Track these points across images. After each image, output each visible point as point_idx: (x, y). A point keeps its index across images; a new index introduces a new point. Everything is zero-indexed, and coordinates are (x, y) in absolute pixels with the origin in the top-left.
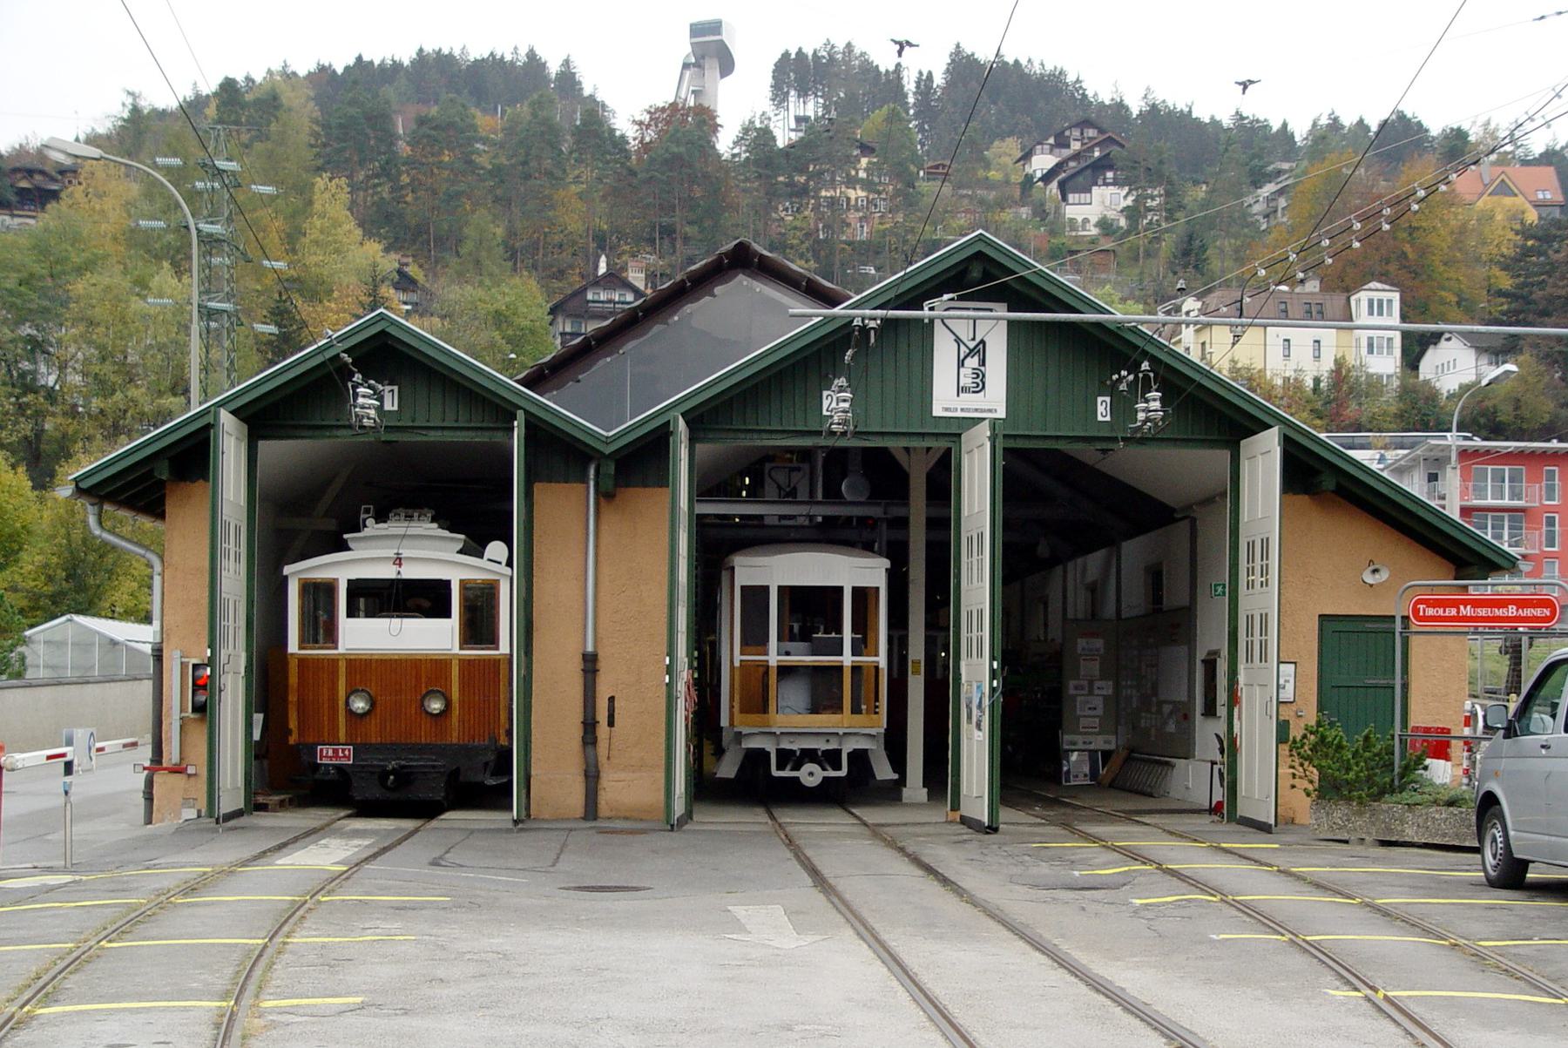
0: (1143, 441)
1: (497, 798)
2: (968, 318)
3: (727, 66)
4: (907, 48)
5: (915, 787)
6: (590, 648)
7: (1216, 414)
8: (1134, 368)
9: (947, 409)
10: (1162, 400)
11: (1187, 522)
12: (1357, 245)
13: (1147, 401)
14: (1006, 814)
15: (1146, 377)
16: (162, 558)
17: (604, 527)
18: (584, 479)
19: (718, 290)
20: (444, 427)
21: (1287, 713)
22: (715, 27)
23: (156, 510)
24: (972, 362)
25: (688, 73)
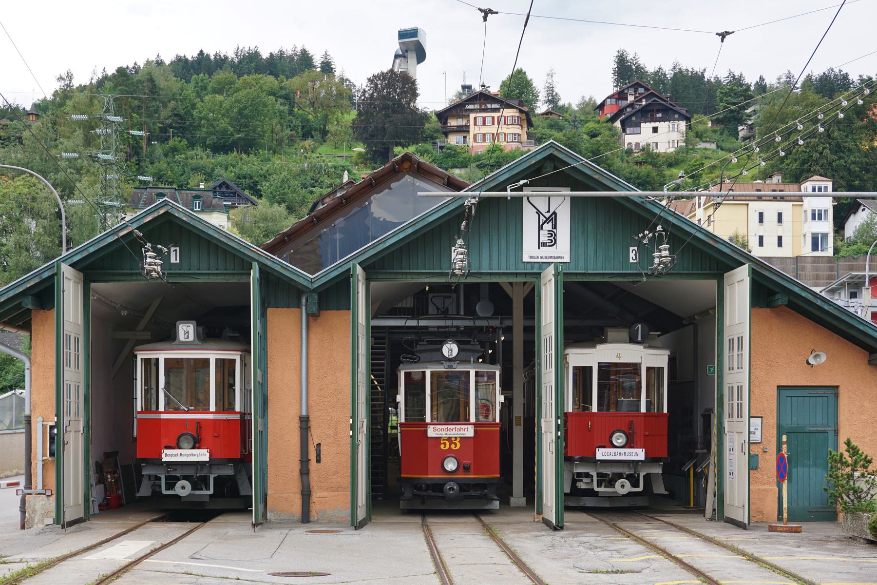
0: (660, 275)
1: (243, 507)
2: (545, 196)
3: (421, 56)
4: (490, 15)
5: (518, 497)
6: (304, 413)
7: (713, 259)
8: (653, 229)
9: (531, 257)
10: (669, 249)
11: (691, 327)
12: (801, 142)
13: (660, 251)
14: (568, 516)
15: (660, 235)
16: (30, 359)
17: (312, 335)
18: (299, 306)
19: (393, 185)
20: (209, 275)
21: (756, 450)
22: (414, 33)
23: (27, 326)
24: (548, 227)
25: (398, 61)
